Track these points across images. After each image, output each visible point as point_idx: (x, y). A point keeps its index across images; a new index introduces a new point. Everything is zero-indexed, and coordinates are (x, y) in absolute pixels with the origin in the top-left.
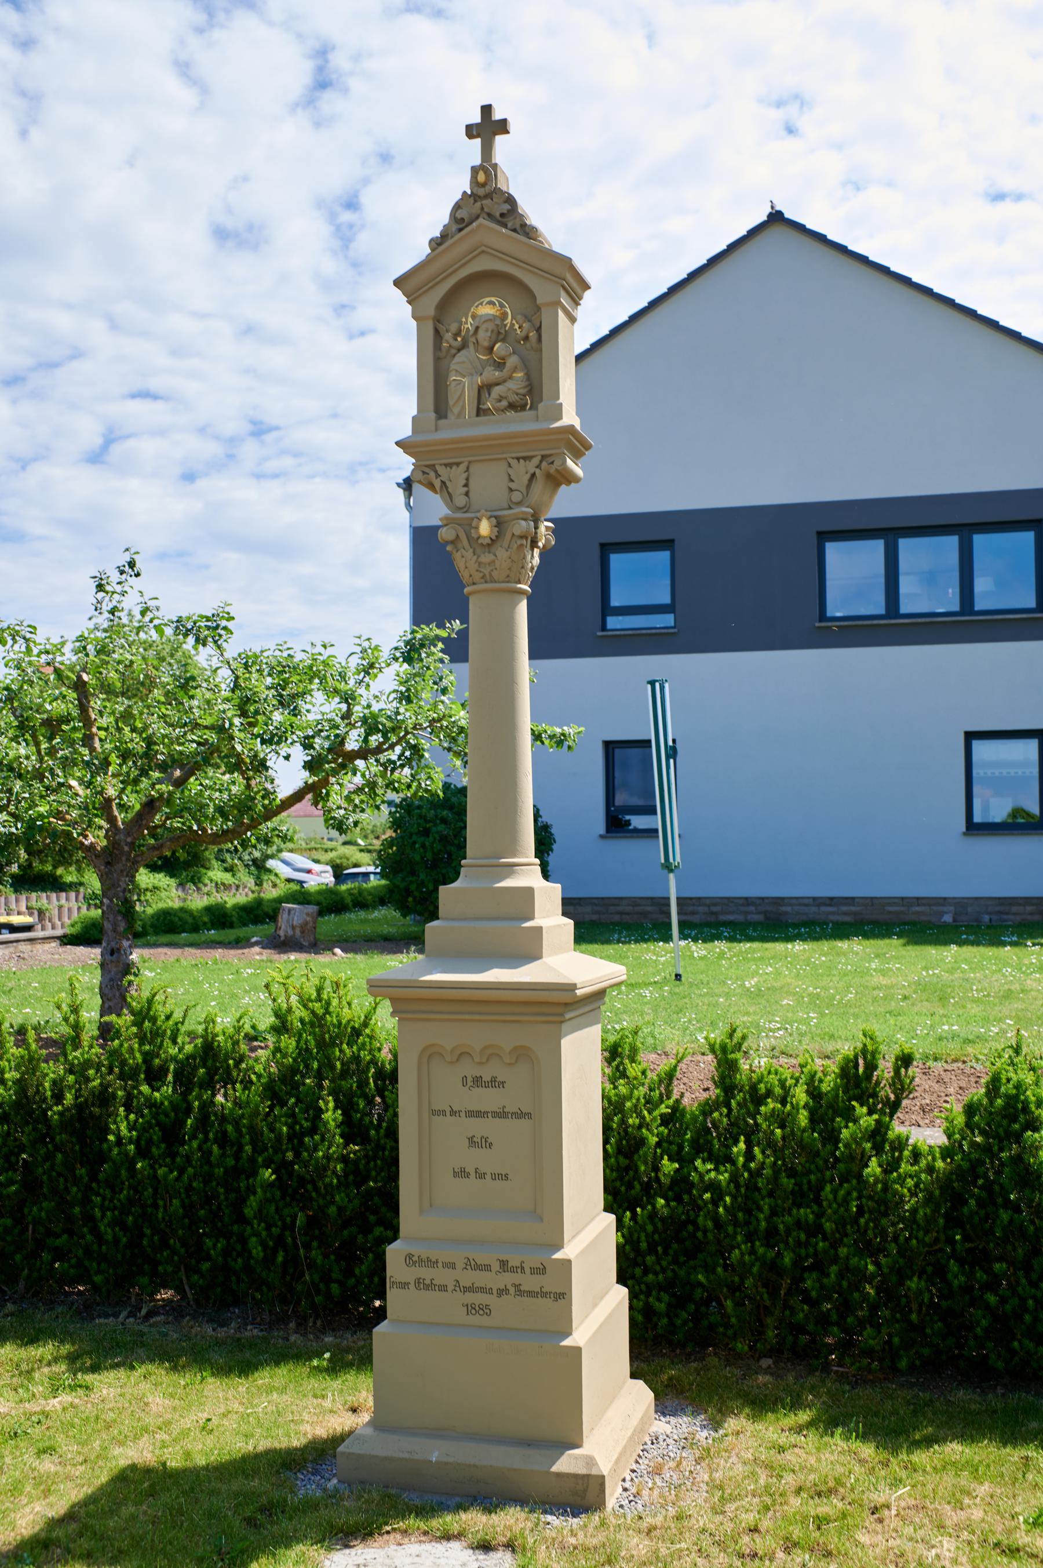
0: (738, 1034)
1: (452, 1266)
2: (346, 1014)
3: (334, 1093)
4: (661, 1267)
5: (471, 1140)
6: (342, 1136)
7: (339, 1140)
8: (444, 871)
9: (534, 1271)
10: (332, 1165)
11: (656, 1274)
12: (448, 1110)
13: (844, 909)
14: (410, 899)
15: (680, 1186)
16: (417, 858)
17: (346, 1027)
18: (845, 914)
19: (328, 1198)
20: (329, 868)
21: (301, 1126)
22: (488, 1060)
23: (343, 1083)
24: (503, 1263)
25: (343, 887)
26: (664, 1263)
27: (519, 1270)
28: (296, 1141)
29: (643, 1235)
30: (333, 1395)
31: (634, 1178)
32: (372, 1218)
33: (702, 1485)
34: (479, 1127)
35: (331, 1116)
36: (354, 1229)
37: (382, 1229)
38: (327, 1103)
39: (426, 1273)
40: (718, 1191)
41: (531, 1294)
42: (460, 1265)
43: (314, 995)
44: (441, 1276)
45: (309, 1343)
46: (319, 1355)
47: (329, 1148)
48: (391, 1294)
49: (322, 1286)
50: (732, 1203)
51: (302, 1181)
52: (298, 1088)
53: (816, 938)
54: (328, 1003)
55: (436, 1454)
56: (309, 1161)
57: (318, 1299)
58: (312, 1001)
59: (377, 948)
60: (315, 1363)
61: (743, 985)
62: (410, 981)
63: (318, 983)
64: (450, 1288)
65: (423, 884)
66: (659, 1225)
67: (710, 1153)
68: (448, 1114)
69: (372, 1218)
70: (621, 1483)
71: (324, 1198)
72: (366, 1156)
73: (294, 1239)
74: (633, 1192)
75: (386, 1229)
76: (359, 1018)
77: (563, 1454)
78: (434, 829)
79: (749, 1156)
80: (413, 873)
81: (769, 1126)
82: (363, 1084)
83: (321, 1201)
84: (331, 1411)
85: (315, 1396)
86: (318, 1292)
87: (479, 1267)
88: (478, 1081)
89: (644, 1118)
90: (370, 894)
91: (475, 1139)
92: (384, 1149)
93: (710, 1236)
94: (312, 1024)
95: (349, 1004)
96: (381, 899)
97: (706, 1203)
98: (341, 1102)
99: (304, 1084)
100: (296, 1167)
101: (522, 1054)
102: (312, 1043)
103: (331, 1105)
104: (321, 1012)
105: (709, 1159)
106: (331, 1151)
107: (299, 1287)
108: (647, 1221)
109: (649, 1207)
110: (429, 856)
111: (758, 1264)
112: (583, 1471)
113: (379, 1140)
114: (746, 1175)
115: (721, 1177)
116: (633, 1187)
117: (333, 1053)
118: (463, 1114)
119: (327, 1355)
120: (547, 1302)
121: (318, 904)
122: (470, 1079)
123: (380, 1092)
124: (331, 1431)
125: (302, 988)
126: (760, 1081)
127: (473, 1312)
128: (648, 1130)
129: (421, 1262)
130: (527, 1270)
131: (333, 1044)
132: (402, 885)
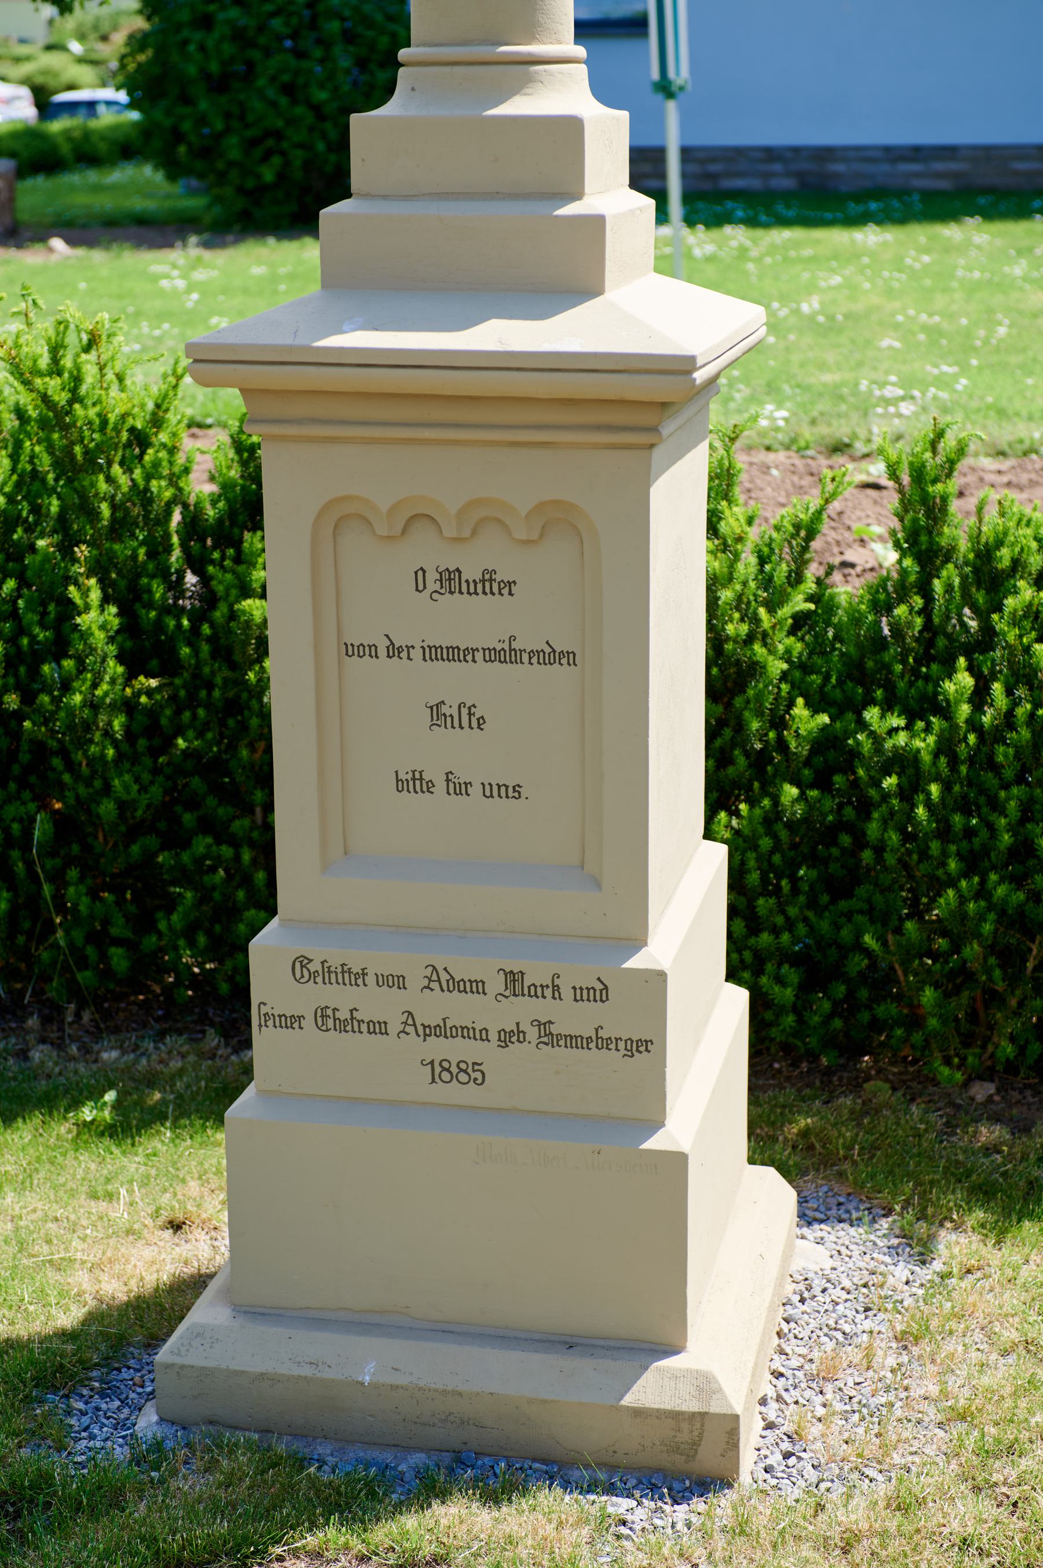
0: (949, 443)
1: (399, 982)
2: (116, 402)
3: (99, 568)
4: (787, 918)
5: (436, 711)
6: (120, 659)
7: (114, 668)
8: (242, 96)
9: (581, 994)
10: (102, 719)
11: (776, 931)
12: (382, 644)
13: (939, 166)
14: (182, 149)
15: (830, 757)
16: (192, 70)
17: (117, 431)
18: (939, 175)
19: (98, 783)
20: (25, 92)
21: (33, 638)
22: (474, 532)
23: (117, 547)
24: (513, 979)
25: (56, 126)
26: (793, 911)
27: (548, 992)
28: (22, 670)
29: (751, 856)
30: (131, 1192)
31: (733, 744)
32: (188, 819)
33: (924, 1406)
34: (452, 683)
35: (96, 619)
36: (152, 841)
37: (209, 840)
38: (85, 593)
39: (341, 998)
40: (910, 771)
41: (573, 1041)
42: (416, 980)
43: (44, 362)
44: (373, 1002)
45: (71, 1066)
46: (95, 1094)
47: (95, 685)
48: (259, 1037)
49: (91, 951)
50: (942, 798)
51: (39, 749)
52: (20, 559)
53: (902, 220)
54: (77, 379)
55: (371, 1367)
56: (54, 713)
57: (85, 977)
58: (41, 374)
59: (127, 239)
60: (87, 1113)
61: (797, 312)
62: (290, 348)
63: (52, 333)
64: (394, 1027)
65: (202, 120)
66: (784, 835)
67: (889, 687)
68: (382, 652)
69: (188, 819)
70: (758, 1408)
71: (89, 785)
72: (174, 698)
73: (29, 865)
74: (731, 770)
75: (219, 842)
76: (142, 406)
77: (646, 1368)
78: (221, 16)
79: (980, 697)
80: (186, 100)
81: (1021, 636)
82: (158, 549)
83: (82, 790)
84: (129, 1232)
85: (94, 1196)
86: (83, 963)
87: (457, 985)
88: (451, 580)
89: (756, 620)
90: (103, 138)
91: (444, 709)
92: (210, 686)
93: (890, 859)
94: (44, 424)
95: (120, 378)
96: (125, 148)
97: (885, 796)
98: (113, 584)
99: (32, 548)
100: (27, 724)
101: (556, 519)
102: (45, 462)
103: (95, 595)
104: (62, 398)
105: (887, 707)
106: (99, 692)
107: (45, 956)
108: (761, 830)
109: (766, 802)
110: (214, 67)
111: (992, 916)
112: (691, 1406)
113: (198, 666)
114: (972, 738)
115: (918, 743)
116: (731, 761)
117: (93, 485)
118: (417, 654)
119: (110, 1096)
120: (613, 1058)
121: (13, 155)
122: (432, 576)
123: (196, 563)
124: (133, 1284)
125: (17, 346)
126: (999, 543)
127: (446, 1076)
128: (765, 645)
129: (327, 973)
130: (567, 993)
131: (91, 464)
132: (168, 122)
